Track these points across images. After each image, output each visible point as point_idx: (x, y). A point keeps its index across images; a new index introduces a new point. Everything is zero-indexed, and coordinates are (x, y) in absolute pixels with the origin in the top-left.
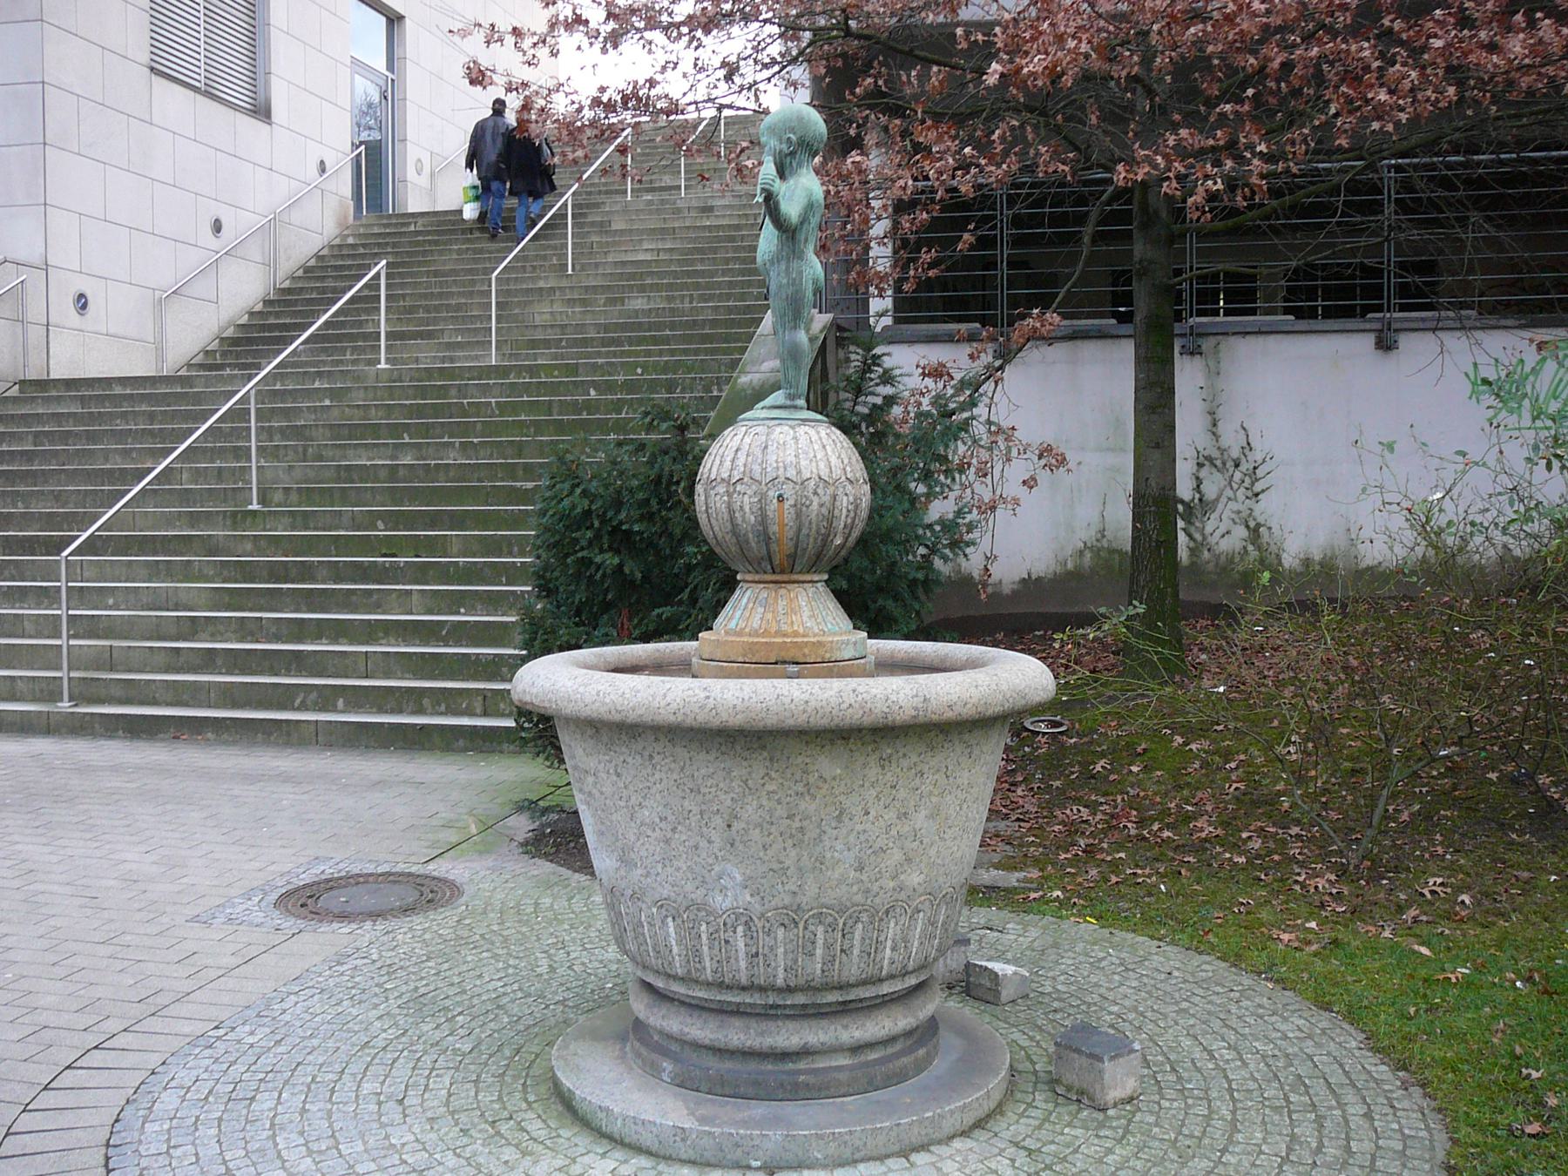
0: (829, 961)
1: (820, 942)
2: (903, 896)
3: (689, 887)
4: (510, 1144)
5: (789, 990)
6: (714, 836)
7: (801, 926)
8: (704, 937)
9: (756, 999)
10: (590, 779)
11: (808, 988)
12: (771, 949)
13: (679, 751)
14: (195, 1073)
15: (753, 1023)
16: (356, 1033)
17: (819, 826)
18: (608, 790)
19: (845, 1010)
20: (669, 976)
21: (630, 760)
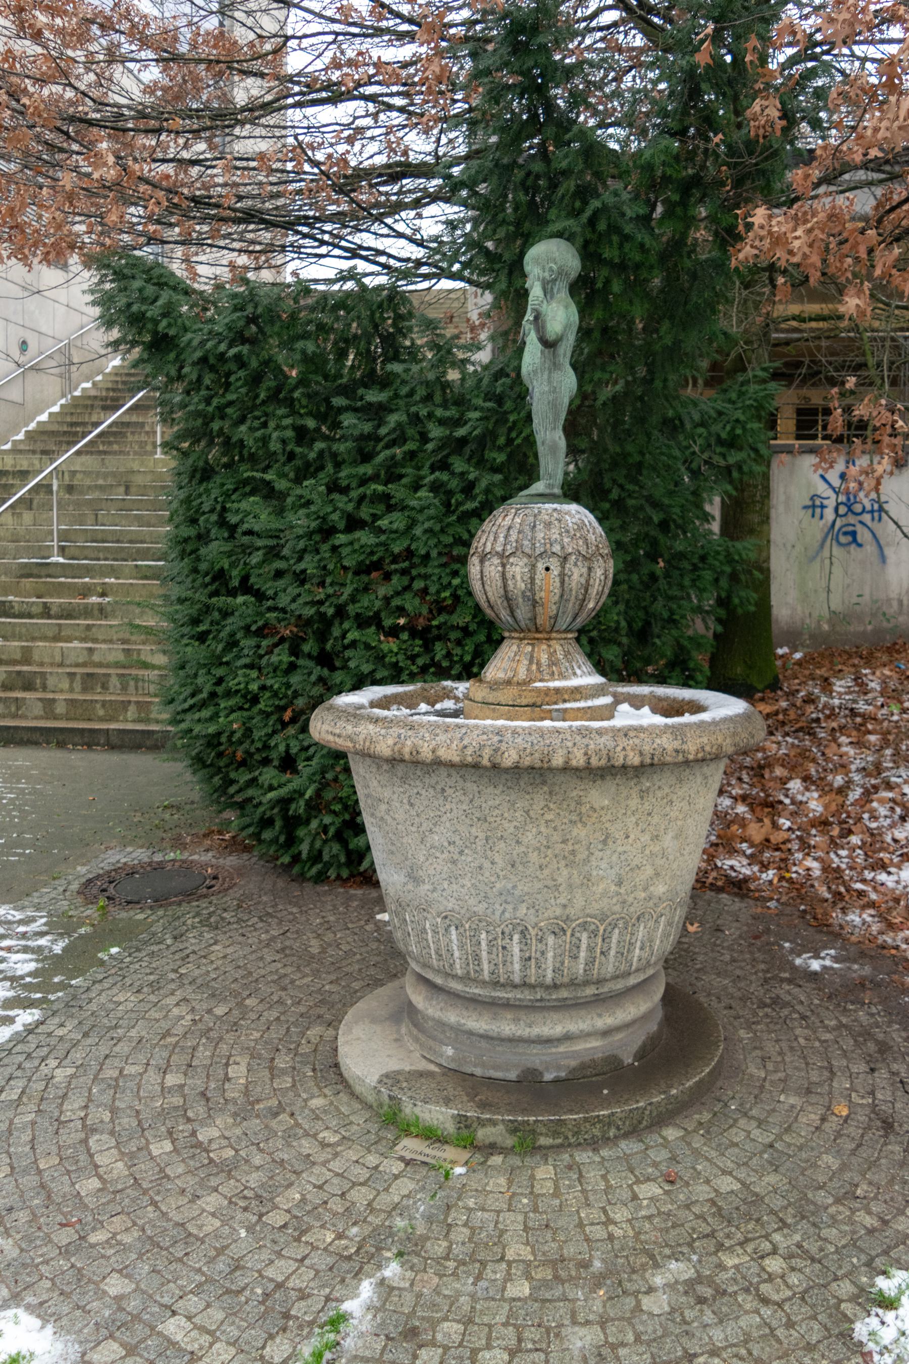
0: (590, 962)
1: (584, 946)
2: (651, 904)
3: (472, 901)
4: (308, 1135)
5: (555, 986)
6: (498, 858)
7: (569, 933)
8: (484, 944)
9: (526, 995)
10: (383, 807)
11: (573, 984)
12: (543, 953)
13: (469, 785)
14: (9, 1070)
15: (522, 1014)
16: (157, 1020)
17: (588, 849)
18: (400, 816)
19: (599, 1001)
20: (447, 975)
21: (423, 792)
